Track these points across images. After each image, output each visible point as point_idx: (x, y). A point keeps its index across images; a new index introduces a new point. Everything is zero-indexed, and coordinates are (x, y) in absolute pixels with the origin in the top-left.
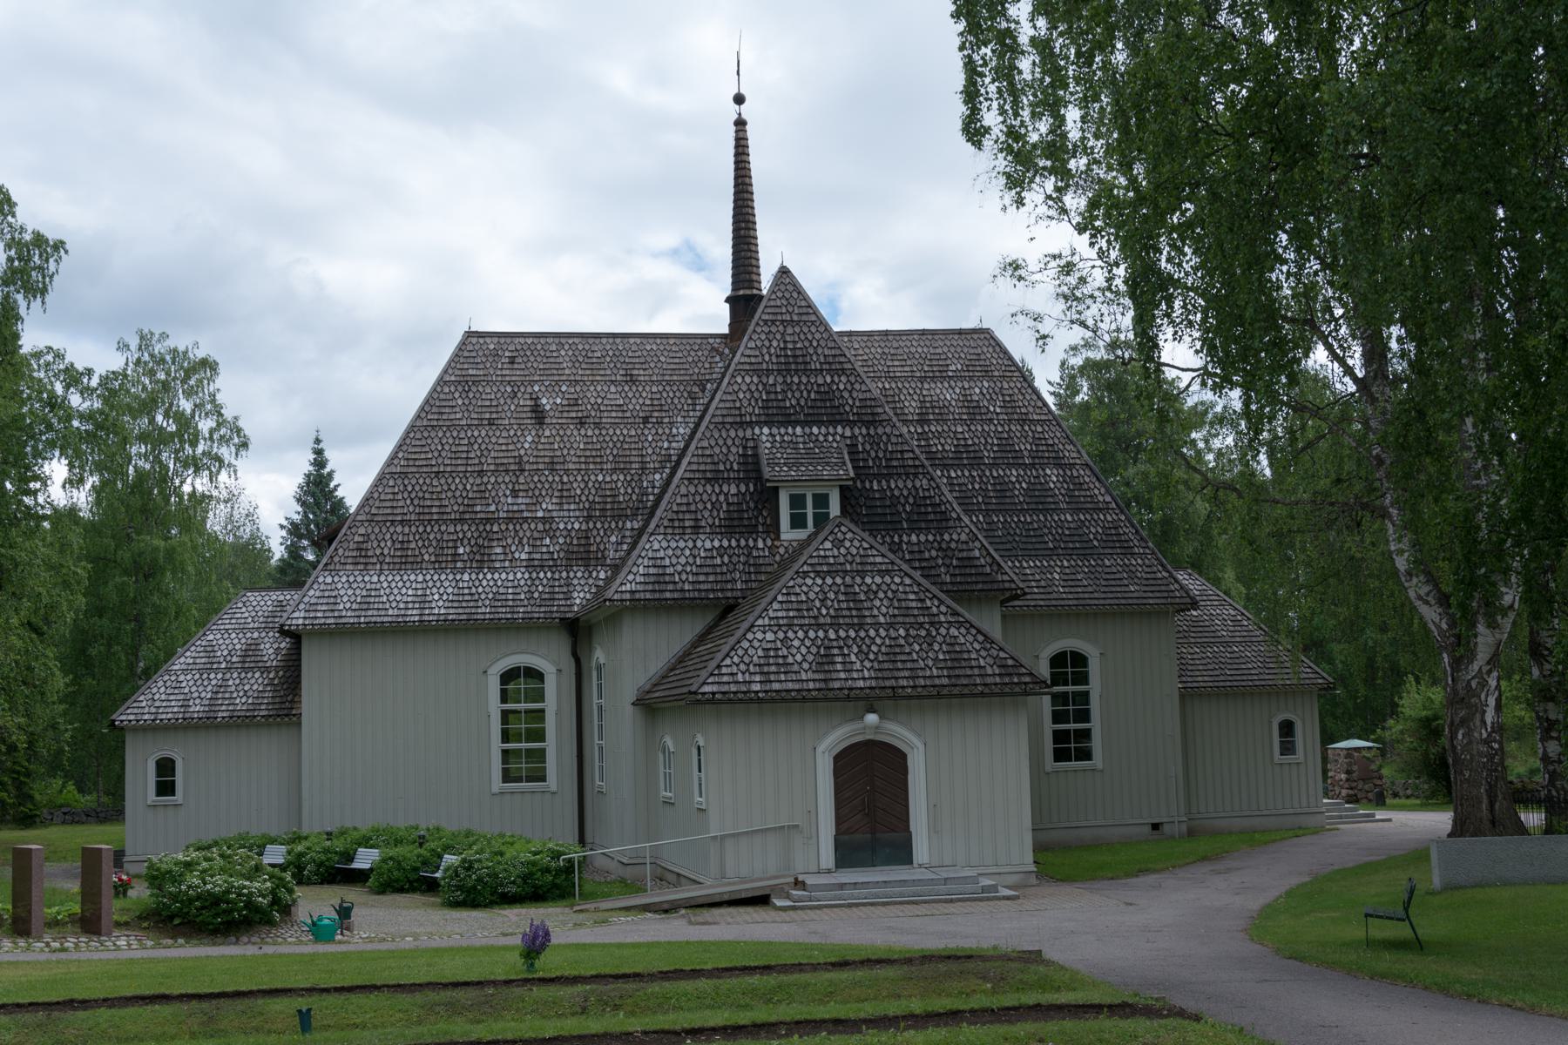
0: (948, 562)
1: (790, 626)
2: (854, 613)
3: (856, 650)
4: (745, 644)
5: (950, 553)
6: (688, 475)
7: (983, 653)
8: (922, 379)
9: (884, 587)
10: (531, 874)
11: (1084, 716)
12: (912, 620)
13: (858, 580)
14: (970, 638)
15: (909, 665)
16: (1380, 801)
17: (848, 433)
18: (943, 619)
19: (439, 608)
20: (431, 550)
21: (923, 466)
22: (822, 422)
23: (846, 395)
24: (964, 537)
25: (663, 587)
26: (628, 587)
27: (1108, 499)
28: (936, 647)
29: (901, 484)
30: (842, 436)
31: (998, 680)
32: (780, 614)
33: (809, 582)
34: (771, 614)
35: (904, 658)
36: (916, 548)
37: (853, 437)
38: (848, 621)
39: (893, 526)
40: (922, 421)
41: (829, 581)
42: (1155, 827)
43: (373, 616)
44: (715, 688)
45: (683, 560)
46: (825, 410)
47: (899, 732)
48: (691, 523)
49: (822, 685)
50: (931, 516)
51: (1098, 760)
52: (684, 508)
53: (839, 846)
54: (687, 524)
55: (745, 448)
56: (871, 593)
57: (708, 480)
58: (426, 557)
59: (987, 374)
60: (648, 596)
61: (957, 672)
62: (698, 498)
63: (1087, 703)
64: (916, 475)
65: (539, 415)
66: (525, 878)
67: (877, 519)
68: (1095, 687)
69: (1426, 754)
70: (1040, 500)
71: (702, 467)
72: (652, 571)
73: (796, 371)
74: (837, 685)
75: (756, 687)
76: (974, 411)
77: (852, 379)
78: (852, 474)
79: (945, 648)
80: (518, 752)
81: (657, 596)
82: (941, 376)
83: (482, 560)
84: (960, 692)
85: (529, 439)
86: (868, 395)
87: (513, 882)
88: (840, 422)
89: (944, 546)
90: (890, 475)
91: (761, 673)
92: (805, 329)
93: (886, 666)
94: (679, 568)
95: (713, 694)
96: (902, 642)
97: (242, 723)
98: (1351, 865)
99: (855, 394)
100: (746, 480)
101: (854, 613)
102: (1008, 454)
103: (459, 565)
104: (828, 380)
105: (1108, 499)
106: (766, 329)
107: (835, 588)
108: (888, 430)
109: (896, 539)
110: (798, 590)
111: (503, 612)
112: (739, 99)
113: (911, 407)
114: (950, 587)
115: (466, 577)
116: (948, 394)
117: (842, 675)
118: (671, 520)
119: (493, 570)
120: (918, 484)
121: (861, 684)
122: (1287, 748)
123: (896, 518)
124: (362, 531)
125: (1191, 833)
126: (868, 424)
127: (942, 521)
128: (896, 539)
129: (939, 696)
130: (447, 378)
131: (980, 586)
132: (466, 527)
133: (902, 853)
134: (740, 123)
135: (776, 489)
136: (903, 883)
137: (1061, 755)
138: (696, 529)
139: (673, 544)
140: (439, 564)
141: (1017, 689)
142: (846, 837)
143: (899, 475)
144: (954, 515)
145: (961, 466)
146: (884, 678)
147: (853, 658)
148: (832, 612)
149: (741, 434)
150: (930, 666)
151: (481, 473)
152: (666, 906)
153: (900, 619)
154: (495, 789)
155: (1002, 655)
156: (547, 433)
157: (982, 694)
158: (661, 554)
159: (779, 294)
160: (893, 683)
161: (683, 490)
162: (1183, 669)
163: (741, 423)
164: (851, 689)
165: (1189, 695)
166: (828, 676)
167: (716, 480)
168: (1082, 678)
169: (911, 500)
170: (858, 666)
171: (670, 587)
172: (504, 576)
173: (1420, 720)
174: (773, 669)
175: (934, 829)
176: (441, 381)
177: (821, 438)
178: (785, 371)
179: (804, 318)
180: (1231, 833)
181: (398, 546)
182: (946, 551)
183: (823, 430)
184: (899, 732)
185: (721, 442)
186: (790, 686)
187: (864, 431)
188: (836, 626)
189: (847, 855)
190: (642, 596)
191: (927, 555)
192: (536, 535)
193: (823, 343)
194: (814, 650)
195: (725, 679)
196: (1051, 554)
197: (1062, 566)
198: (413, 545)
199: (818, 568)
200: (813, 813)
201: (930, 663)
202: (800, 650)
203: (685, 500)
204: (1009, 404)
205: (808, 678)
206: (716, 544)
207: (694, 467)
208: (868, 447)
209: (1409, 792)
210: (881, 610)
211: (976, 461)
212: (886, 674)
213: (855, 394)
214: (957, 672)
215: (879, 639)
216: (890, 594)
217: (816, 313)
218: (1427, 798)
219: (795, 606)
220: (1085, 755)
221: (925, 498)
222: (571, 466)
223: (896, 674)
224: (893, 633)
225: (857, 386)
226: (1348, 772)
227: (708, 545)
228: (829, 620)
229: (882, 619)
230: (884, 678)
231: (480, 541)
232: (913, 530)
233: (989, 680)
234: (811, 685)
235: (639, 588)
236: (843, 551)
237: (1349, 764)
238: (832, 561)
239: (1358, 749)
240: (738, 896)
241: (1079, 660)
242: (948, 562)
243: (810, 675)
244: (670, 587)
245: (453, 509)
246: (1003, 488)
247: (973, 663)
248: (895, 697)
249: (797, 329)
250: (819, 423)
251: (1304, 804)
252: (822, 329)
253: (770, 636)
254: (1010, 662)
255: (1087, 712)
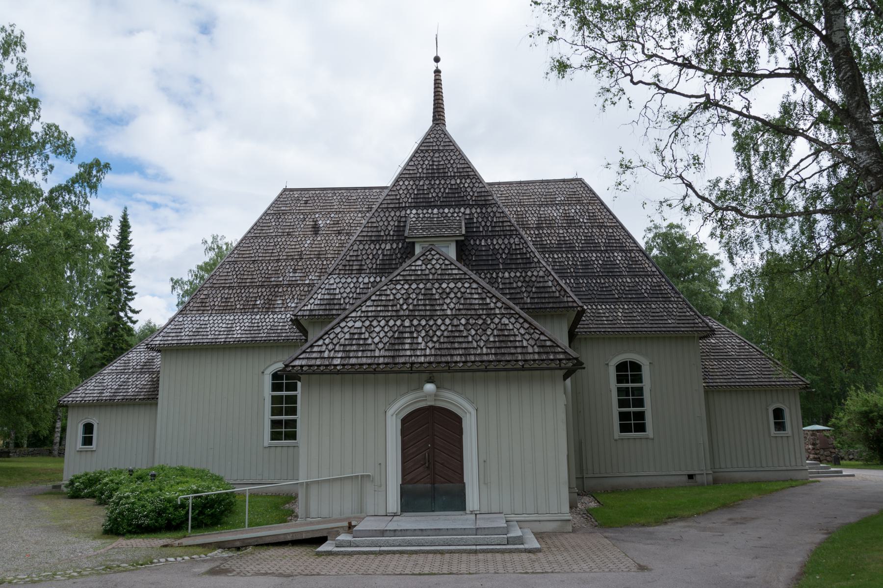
0: (529, 289)
1: (375, 317)
2: (429, 308)
3: (423, 333)
4: (338, 330)
5: (531, 284)
6: (360, 238)
7: (527, 336)
8: (540, 206)
9: (456, 290)
10: (166, 509)
11: (640, 403)
12: (473, 312)
13: (437, 285)
14: (518, 325)
15: (464, 346)
16: (837, 461)
17: (468, 211)
18: (497, 311)
19: (238, 334)
20: (242, 302)
21: (516, 230)
22: (451, 206)
23: (469, 190)
24: (541, 273)
25: (332, 307)
26: (309, 307)
27: (654, 269)
28: (489, 332)
29: (500, 242)
30: (464, 213)
31: (536, 357)
32: (370, 309)
33: (399, 287)
34: (364, 309)
35: (461, 340)
36: (507, 281)
37: (471, 214)
38: (422, 313)
39: (494, 267)
40: (539, 227)
41: (414, 286)
42: (691, 477)
43: (199, 339)
44: (304, 362)
45: (348, 290)
46: (455, 199)
47: (455, 400)
48: (357, 267)
49: (390, 360)
50: (520, 260)
51: (650, 431)
52: (354, 258)
53: (404, 493)
54: (354, 268)
55: (399, 222)
56: (445, 294)
57: (372, 241)
58: (238, 306)
59: (579, 202)
60: (321, 313)
61: (503, 351)
62: (364, 252)
63: (642, 395)
64: (511, 236)
65: (316, 229)
66: (160, 513)
67: (482, 263)
68: (647, 384)
69: (867, 434)
70: (610, 270)
71: (370, 234)
72: (326, 297)
73: (438, 177)
74: (402, 360)
75: (337, 362)
76: (570, 222)
77: (474, 181)
78: (464, 232)
79: (495, 332)
80: (280, 421)
81: (327, 312)
82: (553, 203)
83: (269, 307)
84: (505, 367)
85: (308, 242)
86: (483, 189)
87: (147, 516)
88: (463, 205)
89: (527, 279)
90: (494, 236)
91: (344, 351)
92: (447, 154)
93: (445, 346)
94: (345, 295)
95: (302, 366)
96: (462, 328)
97: (129, 403)
98: (853, 519)
99: (474, 189)
100: (397, 241)
101: (429, 308)
102: (590, 245)
103: (256, 310)
104: (458, 181)
105: (654, 269)
106: (422, 155)
107: (417, 291)
108: (495, 209)
109: (494, 275)
110: (388, 292)
111: (273, 337)
112: (437, 60)
113: (533, 220)
114: (529, 306)
115: (258, 317)
116: (555, 213)
117: (408, 353)
118: (345, 266)
119: (274, 313)
120: (512, 241)
121: (422, 359)
122: (780, 426)
123: (495, 262)
124: (206, 292)
125: (716, 481)
126: (481, 206)
127: (527, 263)
128: (494, 275)
129: (486, 370)
130: (269, 212)
131: (551, 305)
132: (264, 290)
133: (456, 501)
134: (437, 72)
135: (413, 244)
136: (438, 531)
137: (624, 428)
138: (360, 271)
139: (343, 280)
140: (244, 311)
141: (553, 365)
142: (410, 486)
143: (500, 236)
144: (535, 260)
145: (561, 252)
146: (441, 355)
147: (420, 340)
148: (411, 307)
149: (398, 214)
150: (482, 348)
151: (278, 260)
152: (238, 544)
153: (463, 312)
154: (266, 444)
155: (543, 338)
156: (319, 239)
157: (523, 369)
158: (335, 286)
159: (433, 136)
160: (449, 359)
161: (355, 247)
162: (706, 374)
163: (399, 208)
164: (412, 364)
165: (710, 391)
166: (397, 353)
167: (378, 241)
168: (638, 379)
169: (506, 251)
170: (423, 346)
171: (337, 307)
172: (279, 316)
173: (861, 413)
174: (354, 348)
175: (484, 481)
176: (266, 214)
177: (449, 215)
178: (431, 177)
179: (447, 148)
180: (743, 483)
181: (224, 300)
182: (528, 283)
183: (452, 210)
184: (455, 400)
185: (384, 219)
186: (364, 360)
187: (479, 210)
188: (411, 317)
189: (413, 500)
190: (317, 313)
191: (515, 285)
192: (303, 293)
193: (457, 161)
194: (390, 334)
195: (314, 355)
196: (617, 301)
197: (624, 308)
198: (232, 300)
199: (408, 278)
200: (382, 466)
201: (482, 344)
202: (379, 335)
203: (355, 253)
204: (592, 218)
205: (380, 355)
206: (372, 280)
207: (364, 234)
208: (480, 220)
209: (851, 457)
210: (450, 306)
211: (571, 249)
212: (443, 352)
213: (474, 189)
214: (503, 351)
215: (444, 326)
216: (459, 295)
217: (454, 145)
218: (867, 460)
219: (384, 303)
220: (641, 428)
221: (516, 249)
222: (329, 256)
223: (452, 352)
224: (455, 322)
225: (477, 185)
226: (813, 444)
227: (366, 280)
228: (407, 313)
229: (449, 312)
230: (441, 355)
231: (270, 297)
232: (506, 269)
233: (529, 357)
234: (381, 360)
235: (316, 307)
236: (429, 266)
237: (814, 440)
238: (419, 273)
239: (818, 431)
240: (299, 537)
241: (636, 367)
242: (529, 289)
243: (383, 353)
244: (337, 307)
245: (258, 280)
246: (587, 264)
247: (517, 344)
248: (450, 370)
249: (442, 154)
250: (449, 207)
251: (793, 463)
252: (457, 153)
253: (358, 324)
254: (548, 343)
255: (642, 400)
